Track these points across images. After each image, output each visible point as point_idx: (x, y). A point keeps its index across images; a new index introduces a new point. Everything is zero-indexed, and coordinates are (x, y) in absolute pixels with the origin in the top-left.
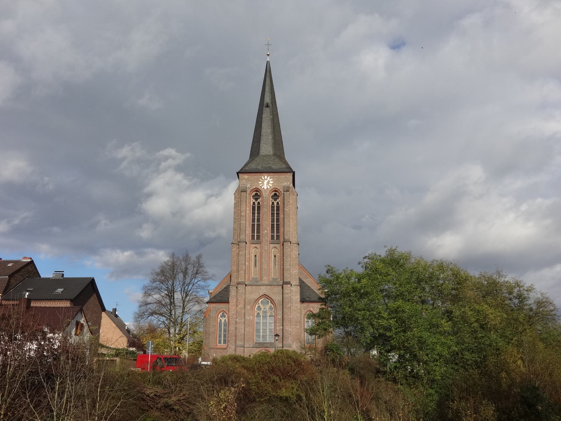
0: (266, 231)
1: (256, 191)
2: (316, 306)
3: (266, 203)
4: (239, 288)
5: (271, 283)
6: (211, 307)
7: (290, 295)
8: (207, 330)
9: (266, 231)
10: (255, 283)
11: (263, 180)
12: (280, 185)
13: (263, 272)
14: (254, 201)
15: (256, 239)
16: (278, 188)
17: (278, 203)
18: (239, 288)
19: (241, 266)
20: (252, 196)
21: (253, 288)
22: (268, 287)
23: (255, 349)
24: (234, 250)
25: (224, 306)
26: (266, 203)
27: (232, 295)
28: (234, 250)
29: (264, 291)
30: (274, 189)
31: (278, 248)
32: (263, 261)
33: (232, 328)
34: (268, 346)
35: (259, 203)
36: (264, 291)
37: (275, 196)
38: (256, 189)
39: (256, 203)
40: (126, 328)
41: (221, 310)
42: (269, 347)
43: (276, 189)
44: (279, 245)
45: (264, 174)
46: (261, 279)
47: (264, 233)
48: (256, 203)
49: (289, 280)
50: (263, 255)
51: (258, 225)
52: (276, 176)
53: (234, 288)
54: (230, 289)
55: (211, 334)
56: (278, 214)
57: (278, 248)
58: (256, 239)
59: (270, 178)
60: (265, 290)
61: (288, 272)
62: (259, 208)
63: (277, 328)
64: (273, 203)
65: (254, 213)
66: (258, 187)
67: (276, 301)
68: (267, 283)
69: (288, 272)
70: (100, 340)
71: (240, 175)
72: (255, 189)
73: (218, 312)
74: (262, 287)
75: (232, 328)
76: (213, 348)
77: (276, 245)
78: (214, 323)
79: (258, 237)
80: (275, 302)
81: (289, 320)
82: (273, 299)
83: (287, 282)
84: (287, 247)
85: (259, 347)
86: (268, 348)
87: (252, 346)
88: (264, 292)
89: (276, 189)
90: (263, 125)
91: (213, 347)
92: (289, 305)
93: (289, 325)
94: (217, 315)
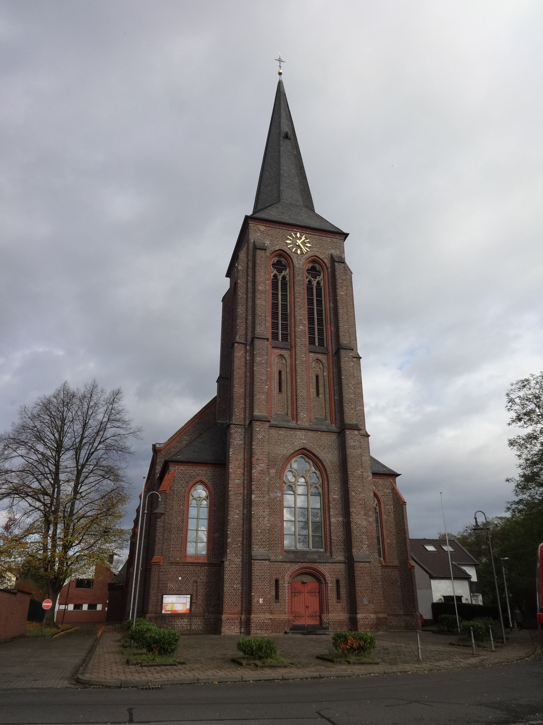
0: (301, 327)
1: (280, 255)
2: (380, 482)
3: (299, 278)
4: (257, 429)
5: (315, 427)
6: (175, 471)
7: (359, 451)
8: (167, 520)
9: (301, 327)
10: (285, 424)
11: (293, 238)
12: (324, 252)
13: (299, 403)
14: (275, 272)
15: (280, 339)
16: (321, 257)
17: (318, 283)
18: (257, 429)
19: (259, 384)
20: (272, 263)
21: (280, 432)
22: (310, 433)
23: (288, 565)
24: (238, 354)
25: (204, 472)
26: (299, 278)
27: (235, 443)
28: (238, 354)
29: (302, 441)
30: (313, 258)
31: (324, 361)
32: (298, 381)
33: (237, 516)
34: (316, 559)
35: (284, 278)
36: (302, 441)
37: (313, 271)
38: (280, 252)
39: (280, 278)
40: (306, 626)
41: (198, 479)
42: (318, 561)
43: (317, 259)
44: (325, 357)
45: (294, 230)
46: (295, 417)
47: (299, 330)
48: (280, 278)
49: (354, 422)
50: (299, 370)
51: (284, 307)
52: (317, 237)
53: (240, 430)
54: (232, 431)
55: (173, 531)
56: (319, 303)
57: (324, 361)
58: (280, 339)
59: (306, 238)
60: (305, 439)
61: (353, 406)
62: (284, 284)
63: (333, 520)
64: (310, 282)
65: (275, 296)
66: (285, 248)
67: (327, 464)
68: (306, 425)
69: (353, 406)
70: (227, 563)
71: (251, 222)
72: (279, 252)
73: (191, 484)
74: (299, 433)
75: (237, 516)
76: (177, 564)
77: (320, 356)
78: (181, 507)
79: (285, 337)
80: (325, 464)
81: (361, 502)
82: (320, 458)
83: (351, 425)
84: (346, 359)
85: (298, 560)
86: (316, 564)
87: (281, 557)
88: (303, 443)
89: (317, 259)
90: (282, 160)
91: (178, 559)
92: (360, 470)
93: (362, 513)
94: (187, 489)
